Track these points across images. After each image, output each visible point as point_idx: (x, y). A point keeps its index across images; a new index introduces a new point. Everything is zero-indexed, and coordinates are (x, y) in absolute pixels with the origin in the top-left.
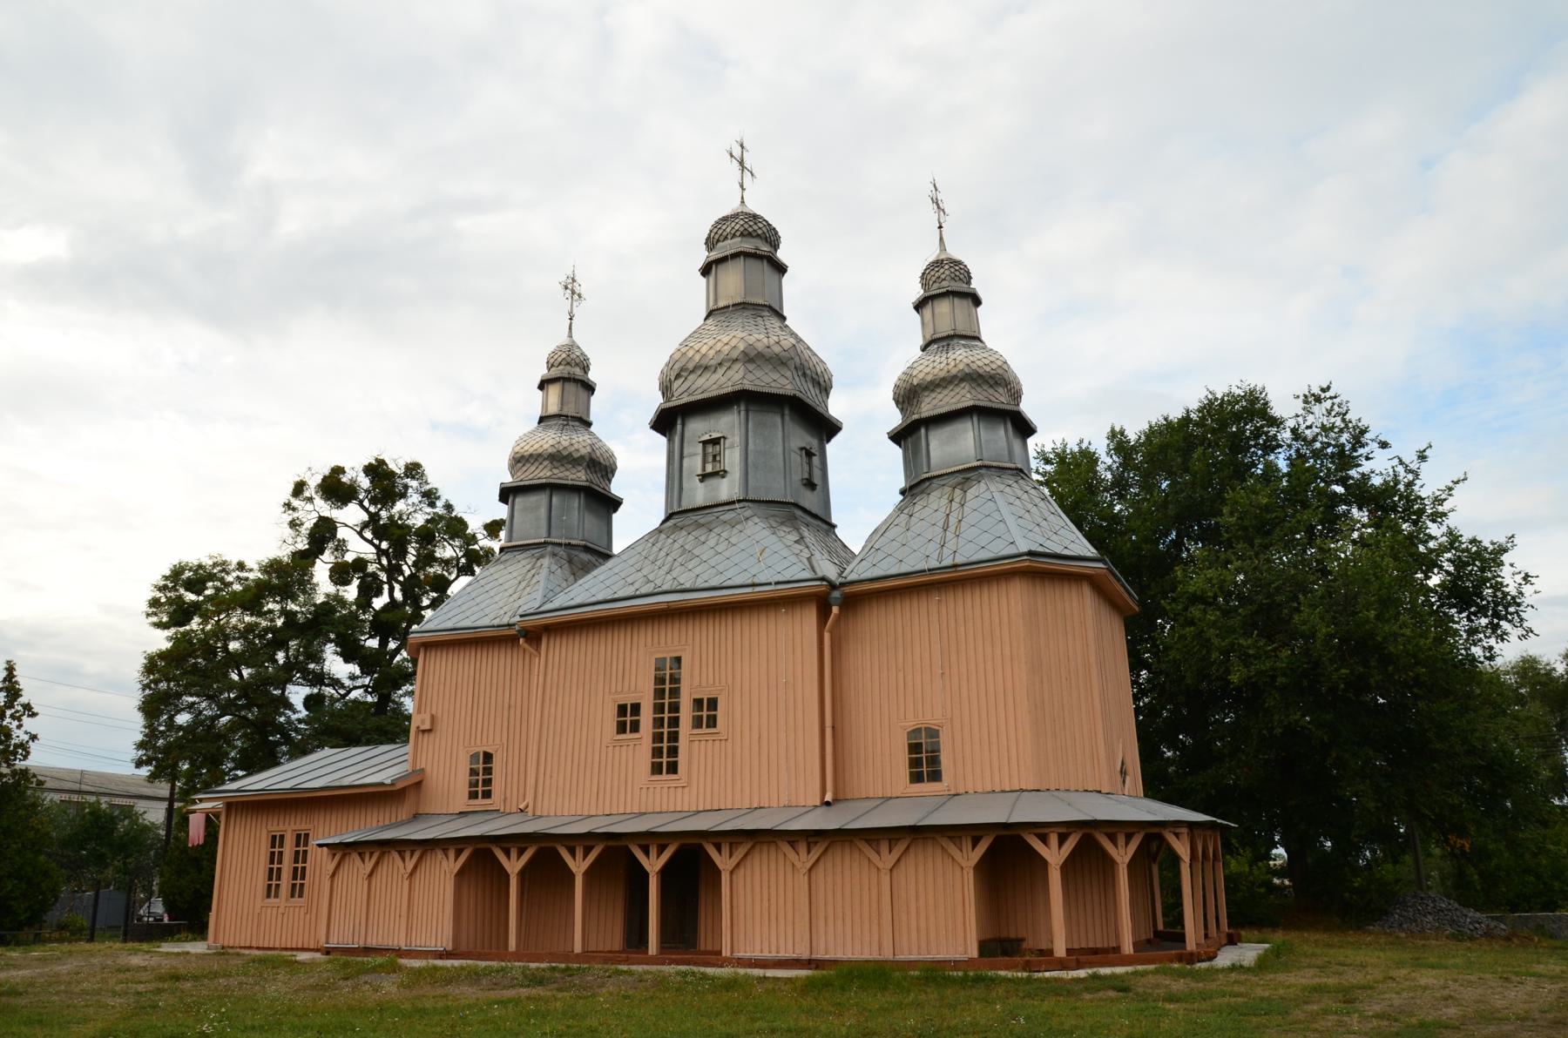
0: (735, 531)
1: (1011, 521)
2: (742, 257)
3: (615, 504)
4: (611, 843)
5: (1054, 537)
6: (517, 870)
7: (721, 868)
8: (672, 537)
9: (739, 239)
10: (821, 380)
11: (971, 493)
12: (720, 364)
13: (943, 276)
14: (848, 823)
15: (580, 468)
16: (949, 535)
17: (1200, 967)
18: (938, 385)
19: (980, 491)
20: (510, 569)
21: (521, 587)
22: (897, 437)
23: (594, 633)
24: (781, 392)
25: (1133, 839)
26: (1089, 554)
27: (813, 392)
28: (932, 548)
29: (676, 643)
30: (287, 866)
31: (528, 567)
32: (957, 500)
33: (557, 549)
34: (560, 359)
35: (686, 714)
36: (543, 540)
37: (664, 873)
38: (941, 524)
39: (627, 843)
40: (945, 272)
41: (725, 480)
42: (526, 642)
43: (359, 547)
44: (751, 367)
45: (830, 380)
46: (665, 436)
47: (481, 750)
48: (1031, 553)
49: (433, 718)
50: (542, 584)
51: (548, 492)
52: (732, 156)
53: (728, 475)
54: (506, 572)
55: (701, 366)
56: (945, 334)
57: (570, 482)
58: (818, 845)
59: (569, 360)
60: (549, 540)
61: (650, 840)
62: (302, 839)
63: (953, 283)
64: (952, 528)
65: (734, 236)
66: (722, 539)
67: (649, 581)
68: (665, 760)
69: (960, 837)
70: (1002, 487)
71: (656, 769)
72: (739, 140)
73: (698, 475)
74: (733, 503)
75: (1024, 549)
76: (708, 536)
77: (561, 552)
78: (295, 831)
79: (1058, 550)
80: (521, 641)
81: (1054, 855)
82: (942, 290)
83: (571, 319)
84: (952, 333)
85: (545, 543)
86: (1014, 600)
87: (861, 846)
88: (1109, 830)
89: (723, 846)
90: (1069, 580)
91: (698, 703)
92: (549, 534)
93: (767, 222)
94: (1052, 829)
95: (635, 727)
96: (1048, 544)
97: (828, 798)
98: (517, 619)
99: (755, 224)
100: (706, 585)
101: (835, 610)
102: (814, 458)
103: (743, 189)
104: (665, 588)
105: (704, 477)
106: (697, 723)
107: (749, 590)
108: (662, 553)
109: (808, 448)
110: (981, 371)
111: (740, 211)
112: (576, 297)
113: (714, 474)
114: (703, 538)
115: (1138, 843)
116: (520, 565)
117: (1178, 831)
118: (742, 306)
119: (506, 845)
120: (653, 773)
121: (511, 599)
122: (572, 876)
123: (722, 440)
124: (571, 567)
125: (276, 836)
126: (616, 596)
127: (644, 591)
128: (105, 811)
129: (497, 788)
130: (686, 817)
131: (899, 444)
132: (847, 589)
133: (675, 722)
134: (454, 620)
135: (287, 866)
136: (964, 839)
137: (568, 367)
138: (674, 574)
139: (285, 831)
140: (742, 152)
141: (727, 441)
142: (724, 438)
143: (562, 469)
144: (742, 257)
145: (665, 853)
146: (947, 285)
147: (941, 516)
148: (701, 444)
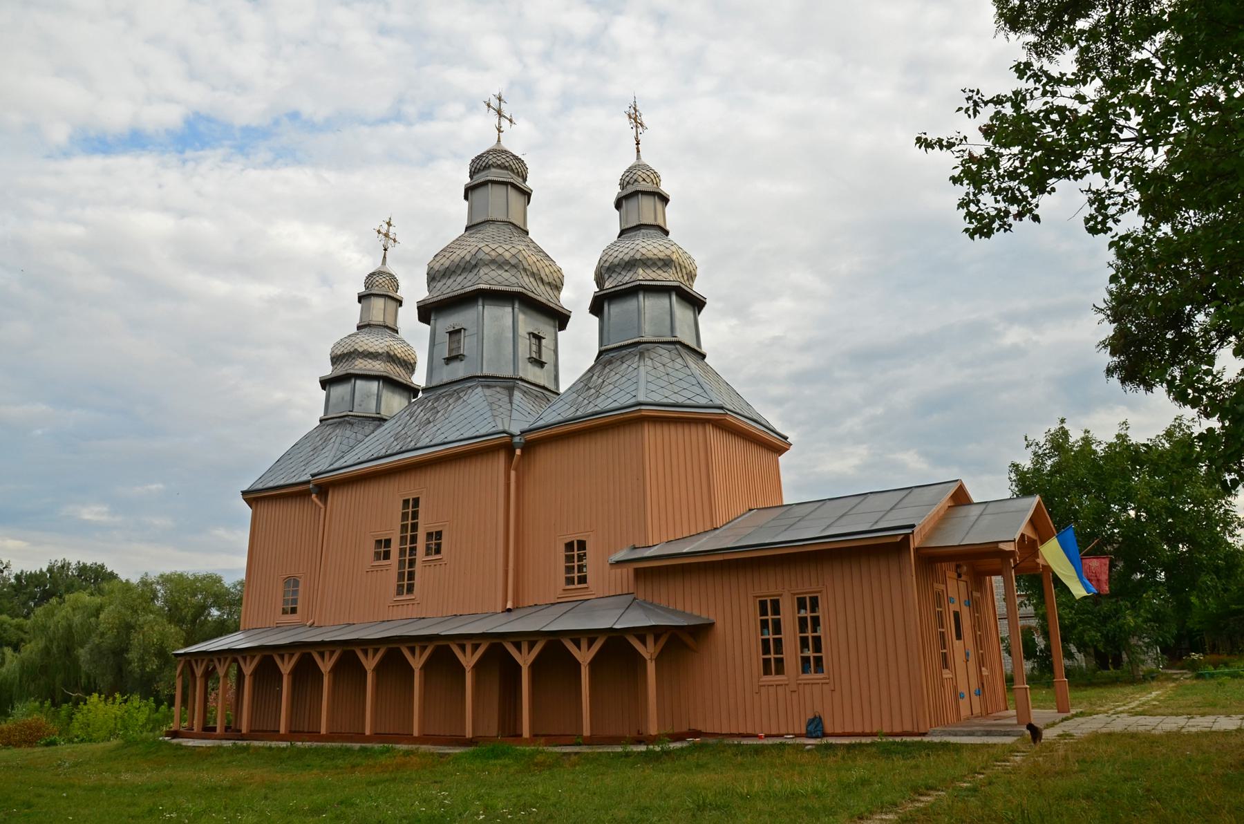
2: (640, 196)
4: (551, 638)
6: (529, 662)
7: (283, 673)
14: (544, 627)
23: (292, 503)
25: (595, 643)
29: (412, 488)
30: (790, 635)
39: (353, 648)
40: (380, 279)
42: (317, 497)
52: (489, 105)
68: (406, 582)
72: (497, 94)
73: (444, 359)
78: (757, 597)
80: (314, 496)
83: (385, 250)
89: (369, 651)
91: (429, 535)
92: (353, 407)
93: (513, 156)
95: (387, 556)
97: (509, 606)
103: (500, 131)
109: (536, 332)
111: (495, 148)
112: (633, 116)
119: (411, 645)
123: (463, 331)
128: (209, 614)
130: (407, 624)
133: (413, 550)
135: (790, 635)
139: (820, 592)
140: (500, 104)
141: (467, 332)
142: (465, 329)
144: (490, 185)
145: (478, 651)
146: (630, 189)
148: (448, 334)
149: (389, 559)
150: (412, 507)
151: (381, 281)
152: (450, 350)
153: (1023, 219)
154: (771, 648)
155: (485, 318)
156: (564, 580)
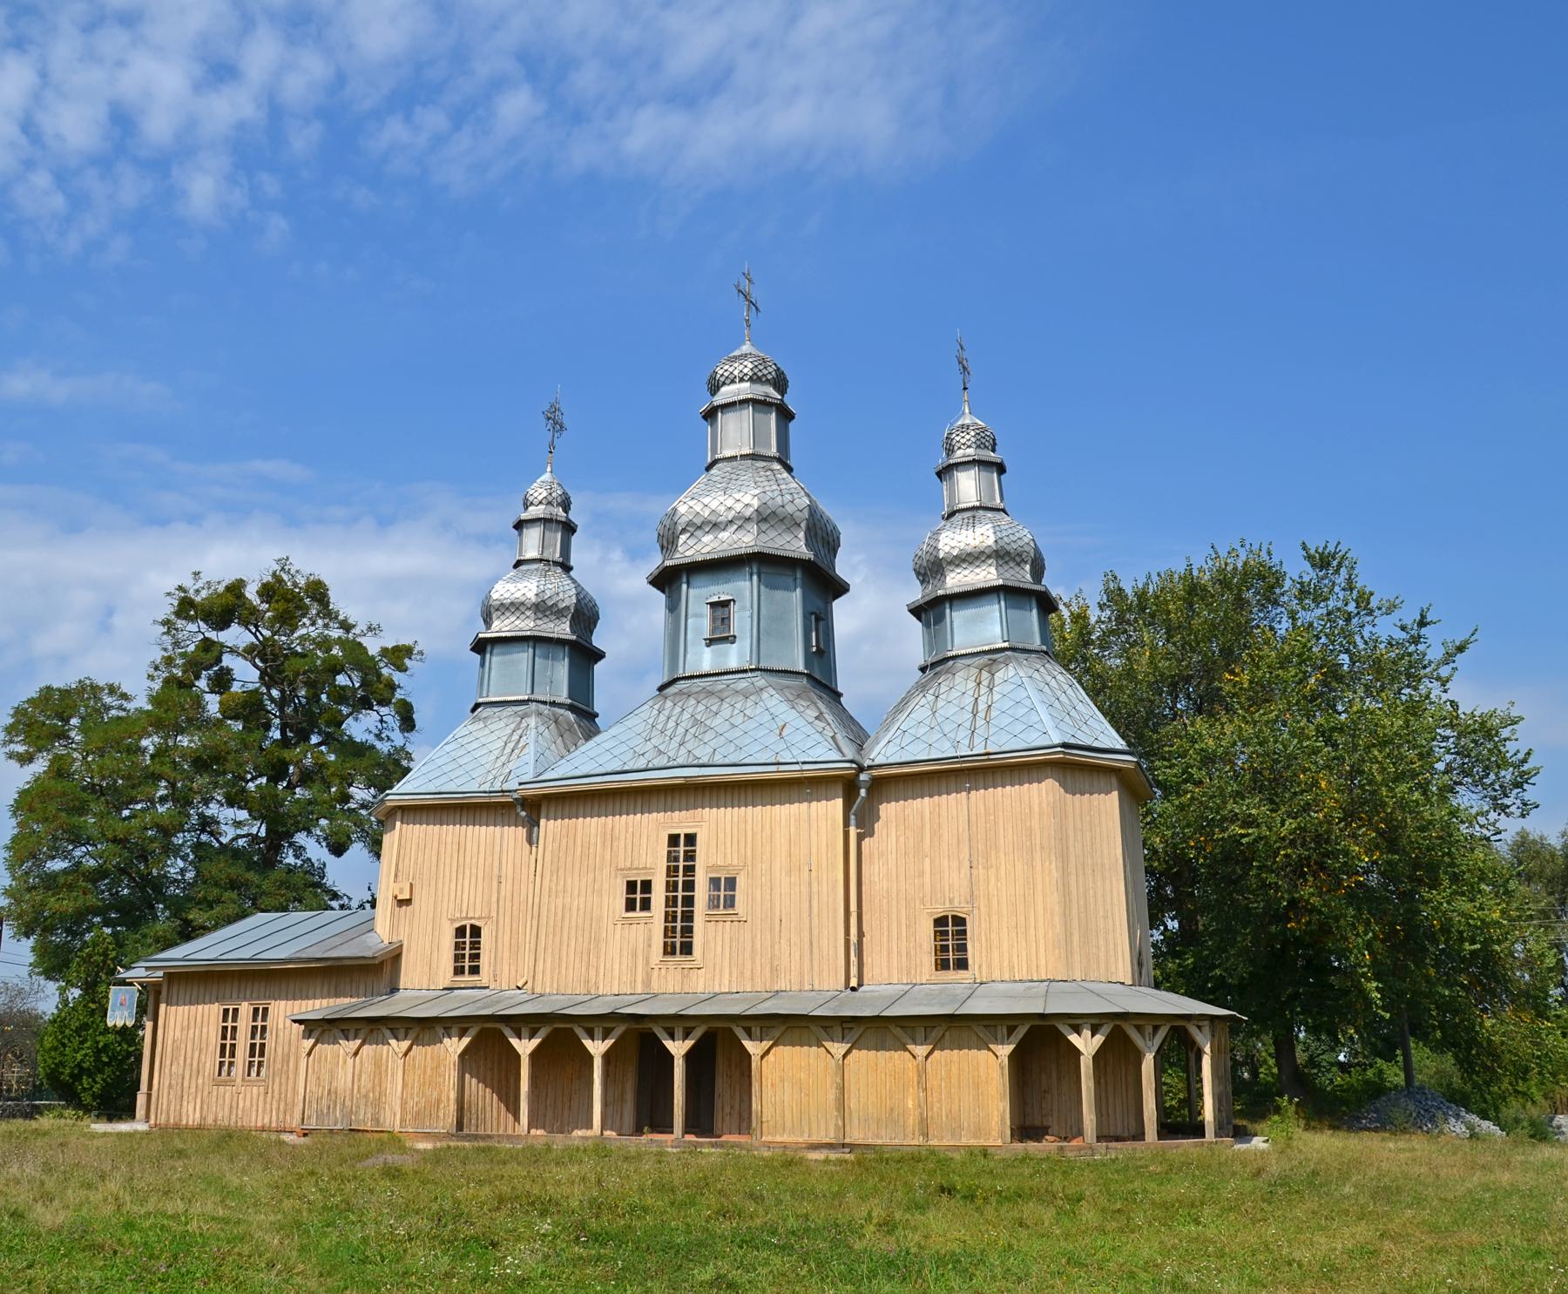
0: (749, 703)
1: (1041, 709)
3: (598, 655)
5: (1084, 728)
6: (529, 1051)
8: (679, 704)
9: (748, 384)
10: (831, 540)
11: (999, 676)
12: (731, 522)
13: (969, 443)
15: (564, 620)
16: (980, 722)
17: (1239, 1150)
18: (964, 561)
19: (1009, 674)
20: (493, 727)
21: (508, 750)
22: (917, 611)
24: (796, 555)
26: (1118, 747)
27: (822, 552)
28: (963, 734)
30: (243, 1042)
31: (512, 726)
32: (985, 683)
33: (542, 706)
34: (540, 498)
35: (701, 894)
36: (526, 698)
37: (689, 1056)
38: (970, 708)
39: (650, 1025)
41: (734, 645)
43: (246, 674)
44: (764, 527)
45: (838, 538)
46: (663, 591)
47: (468, 923)
48: (1065, 745)
49: (411, 884)
50: (532, 746)
51: (531, 644)
53: (737, 639)
54: (487, 731)
55: (710, 522)
56: (970, 505)
57: (556, 636)
58: (853, 1031)
59: (550, 499)
60: (533, 697)
61: (677, 1023)
62: (260, 1013)
63: (980, 451)
64: (981, 715)
65: (742, 380)
66: (736, 712)
67: (660, 752)
68: (679, 942)
69: (996, 1026)
70: (1030, 672)
71: (669, 950)
73: (705, 639)
74: (745, 671)
75: (1057, 741)
76: (720, 705)
77: (545, 709)
79: (1088, 742)
81: (1086, 1044)
82: (966, 459)
84: (978, 504)
85: (528, 700)
86: (1045, 792)
87: (976, 1029)
88: (747, 1024)
90: (1098, 772)
94: (1085, 1021)
95: (646, 905)
96: (1079, 734)
98: (516, 786)
99: (765, 368)
100: (727, 761)
101: (863, 792)
102: (819, 622)
104: (680, 761)
105: (711, 642)
106: (713, 903)
107: (774, 768)
108: (671, 724)
110: (1008, 548)
113: (725, 640)
114: (714, 708)
115: (1109, 1030)
116: (502, 724)
117: (1201, 1024)
118: (754, 457)
120: (665, 953)
121: (499, 763)
122: (591, 1058)
124: (557, 727)
125: (228, 1010)
126: (626, 768)
127: (657, 763)
129: (484, 962)
131: (919, 619)
132: (875, 773)
133: (689, 901)
134: (437, 782)
135: (243, 1042)
136: (999, 1027)
137: (550, 508)
138: (689, 746)
143: (546, 620)
147: (969, 700)
149: (472, 650)
150: (683, 846)
151: (963, 441)
152: (713, 631)
153: (288, 759)
154: (227, 1051)
155: (761, 617)
156: (452, 970)
